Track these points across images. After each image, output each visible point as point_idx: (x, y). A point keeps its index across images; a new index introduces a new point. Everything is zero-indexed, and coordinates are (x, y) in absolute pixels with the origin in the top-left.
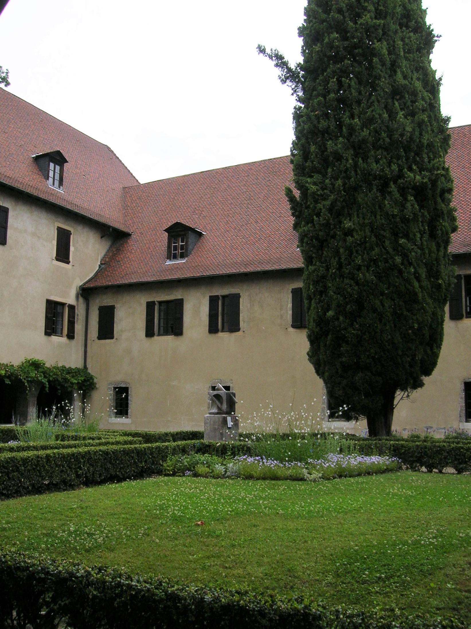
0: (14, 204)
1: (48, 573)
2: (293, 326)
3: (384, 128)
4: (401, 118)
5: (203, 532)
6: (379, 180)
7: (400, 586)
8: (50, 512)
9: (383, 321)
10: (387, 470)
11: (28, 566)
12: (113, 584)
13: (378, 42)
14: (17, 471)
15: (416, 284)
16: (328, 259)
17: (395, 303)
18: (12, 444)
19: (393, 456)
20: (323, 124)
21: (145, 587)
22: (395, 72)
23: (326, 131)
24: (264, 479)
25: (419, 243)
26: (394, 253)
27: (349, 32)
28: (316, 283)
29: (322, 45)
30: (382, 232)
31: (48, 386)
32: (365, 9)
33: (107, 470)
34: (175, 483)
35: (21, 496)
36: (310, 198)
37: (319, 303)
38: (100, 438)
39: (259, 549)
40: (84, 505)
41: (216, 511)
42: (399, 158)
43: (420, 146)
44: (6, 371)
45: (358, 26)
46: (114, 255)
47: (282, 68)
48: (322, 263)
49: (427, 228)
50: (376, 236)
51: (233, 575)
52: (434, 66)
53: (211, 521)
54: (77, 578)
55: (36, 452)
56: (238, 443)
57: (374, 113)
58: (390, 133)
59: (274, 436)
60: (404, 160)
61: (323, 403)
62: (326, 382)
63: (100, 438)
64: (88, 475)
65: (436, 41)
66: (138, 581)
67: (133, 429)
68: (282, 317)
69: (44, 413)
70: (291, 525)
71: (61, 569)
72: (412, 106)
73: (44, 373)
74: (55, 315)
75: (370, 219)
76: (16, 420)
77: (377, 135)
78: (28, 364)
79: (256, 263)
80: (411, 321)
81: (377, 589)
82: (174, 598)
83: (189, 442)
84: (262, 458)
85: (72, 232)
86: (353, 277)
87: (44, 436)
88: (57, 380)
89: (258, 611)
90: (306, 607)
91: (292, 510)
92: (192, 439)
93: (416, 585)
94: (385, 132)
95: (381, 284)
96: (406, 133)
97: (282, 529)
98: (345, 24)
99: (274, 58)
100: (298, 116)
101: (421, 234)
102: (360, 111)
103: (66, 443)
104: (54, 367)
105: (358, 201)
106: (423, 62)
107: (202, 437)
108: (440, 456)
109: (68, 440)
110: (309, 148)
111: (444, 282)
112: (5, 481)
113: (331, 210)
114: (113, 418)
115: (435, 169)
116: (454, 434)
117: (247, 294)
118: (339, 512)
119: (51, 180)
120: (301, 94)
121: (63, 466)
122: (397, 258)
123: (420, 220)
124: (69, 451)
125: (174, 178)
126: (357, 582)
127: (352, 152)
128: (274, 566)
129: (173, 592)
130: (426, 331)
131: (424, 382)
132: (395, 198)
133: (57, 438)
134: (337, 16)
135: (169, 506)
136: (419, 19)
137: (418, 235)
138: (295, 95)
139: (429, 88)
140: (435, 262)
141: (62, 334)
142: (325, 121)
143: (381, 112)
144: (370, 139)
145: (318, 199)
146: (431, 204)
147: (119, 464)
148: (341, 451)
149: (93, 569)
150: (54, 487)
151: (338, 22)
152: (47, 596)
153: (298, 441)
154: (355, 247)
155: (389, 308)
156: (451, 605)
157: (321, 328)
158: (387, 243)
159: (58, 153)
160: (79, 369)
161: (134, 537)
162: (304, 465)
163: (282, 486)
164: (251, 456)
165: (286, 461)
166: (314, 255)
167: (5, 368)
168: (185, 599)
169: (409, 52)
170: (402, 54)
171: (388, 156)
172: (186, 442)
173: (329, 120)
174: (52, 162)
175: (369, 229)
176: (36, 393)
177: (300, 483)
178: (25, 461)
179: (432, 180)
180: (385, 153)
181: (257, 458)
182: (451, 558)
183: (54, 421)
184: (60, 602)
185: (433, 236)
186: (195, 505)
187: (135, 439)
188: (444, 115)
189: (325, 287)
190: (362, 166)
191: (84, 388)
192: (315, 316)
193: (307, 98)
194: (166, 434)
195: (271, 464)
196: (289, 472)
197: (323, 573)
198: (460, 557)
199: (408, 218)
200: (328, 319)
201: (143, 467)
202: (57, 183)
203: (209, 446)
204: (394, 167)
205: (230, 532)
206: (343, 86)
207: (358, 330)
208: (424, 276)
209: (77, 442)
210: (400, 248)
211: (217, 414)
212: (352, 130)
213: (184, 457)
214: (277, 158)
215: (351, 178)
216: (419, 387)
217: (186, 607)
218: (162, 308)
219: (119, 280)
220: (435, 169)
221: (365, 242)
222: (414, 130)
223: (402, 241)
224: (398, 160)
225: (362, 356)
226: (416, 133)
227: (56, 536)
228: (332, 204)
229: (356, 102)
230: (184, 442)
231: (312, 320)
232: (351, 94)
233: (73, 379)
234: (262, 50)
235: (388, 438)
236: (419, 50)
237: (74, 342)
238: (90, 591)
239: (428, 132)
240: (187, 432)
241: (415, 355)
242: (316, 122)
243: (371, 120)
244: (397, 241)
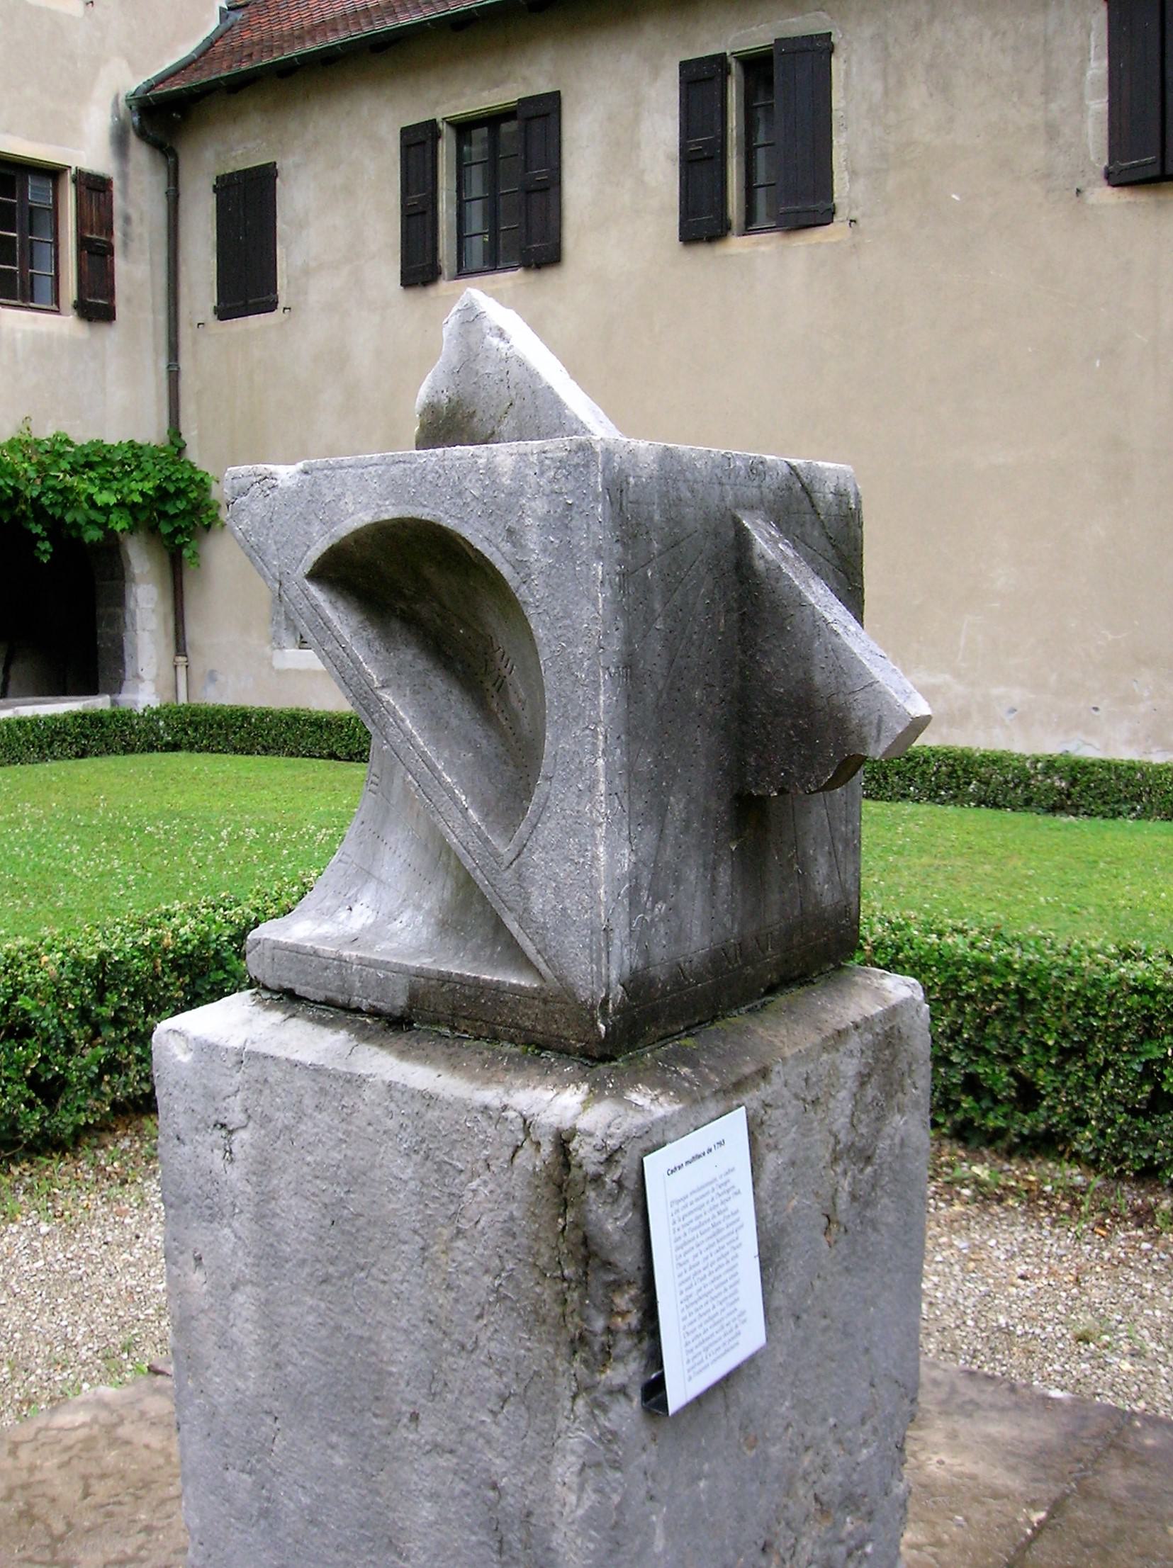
2: (1116, 178)
117: (868, 31)
218: (477, 149)
234: (721, 1143)
237: (111, 336)
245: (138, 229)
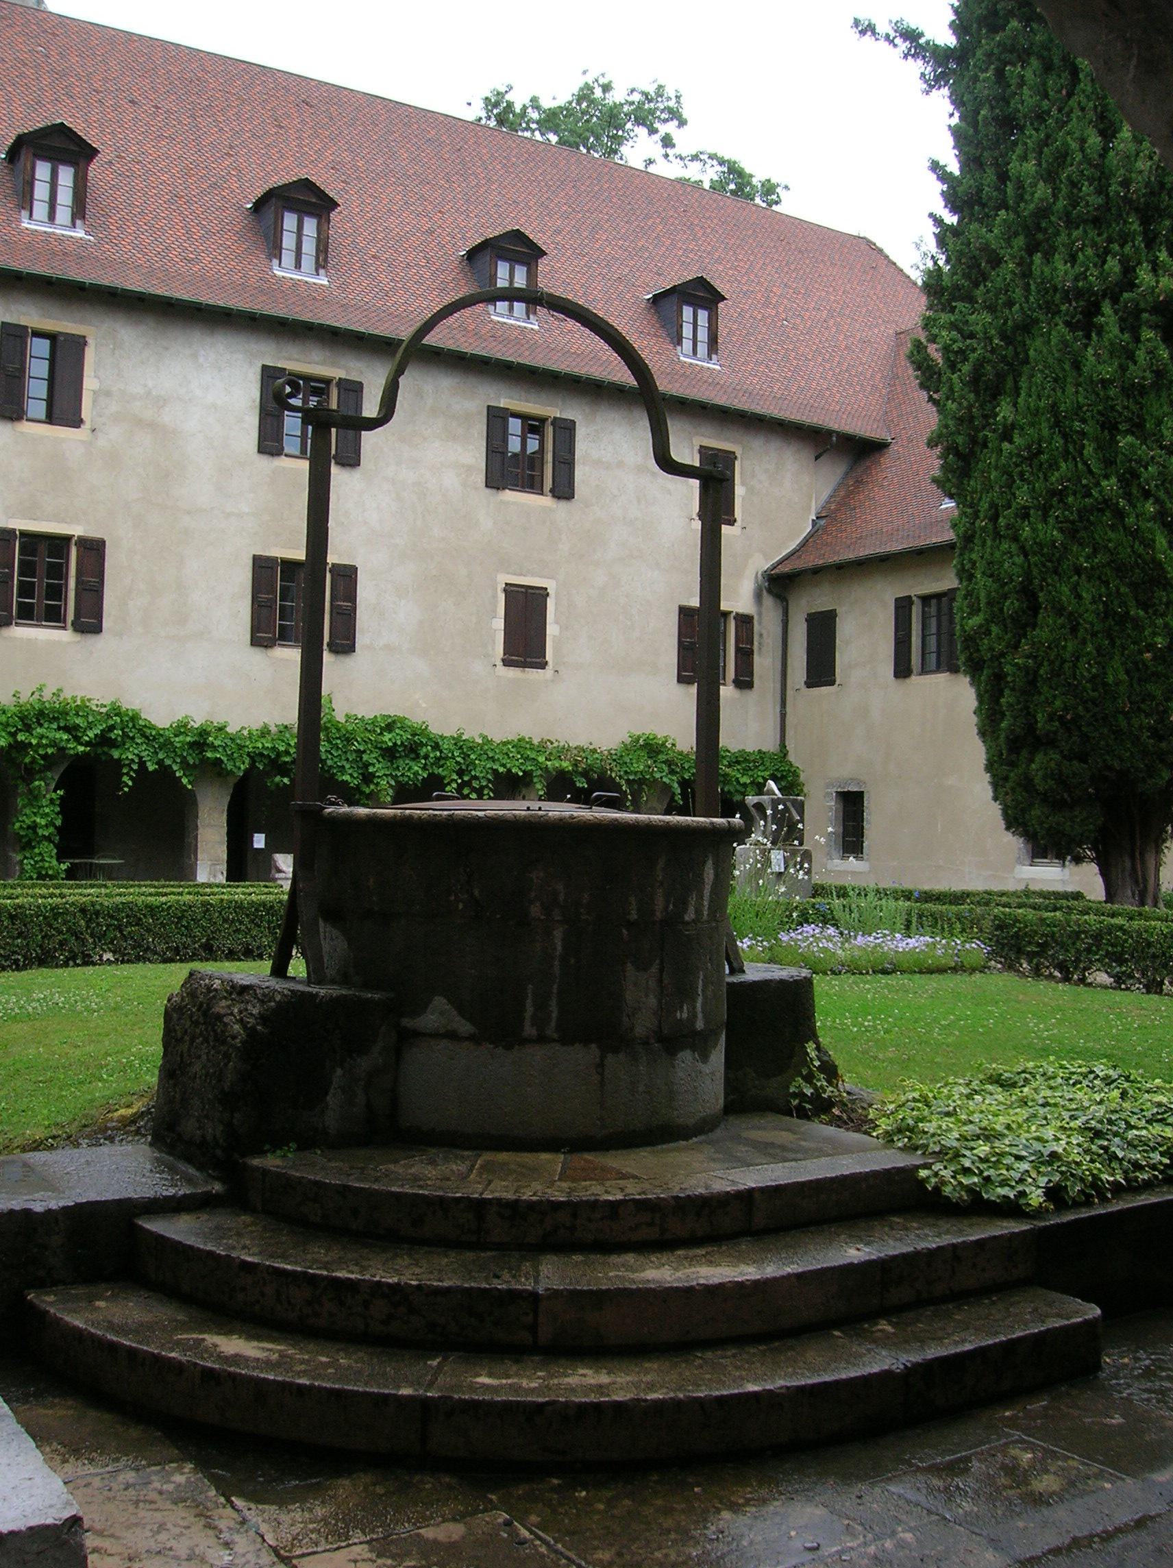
0: (587, 410)
6: (1077, 299)
42: (1124, 239)
50: (1065, 436)
73: (669, 763)
114: (837, 861)
119: (687, 345)
158: (1089, 449)
159: (701, 282)
174: (689, 304)
175: (1048, 420)
180: (1092, 233)
202: (702, 349)
204: (1113, 264)
221: (1040, 452)
223: (1125, 441)
224: (1122, 246)
234: (867, 29)
237: (751, 696)
244: (1114, 441)
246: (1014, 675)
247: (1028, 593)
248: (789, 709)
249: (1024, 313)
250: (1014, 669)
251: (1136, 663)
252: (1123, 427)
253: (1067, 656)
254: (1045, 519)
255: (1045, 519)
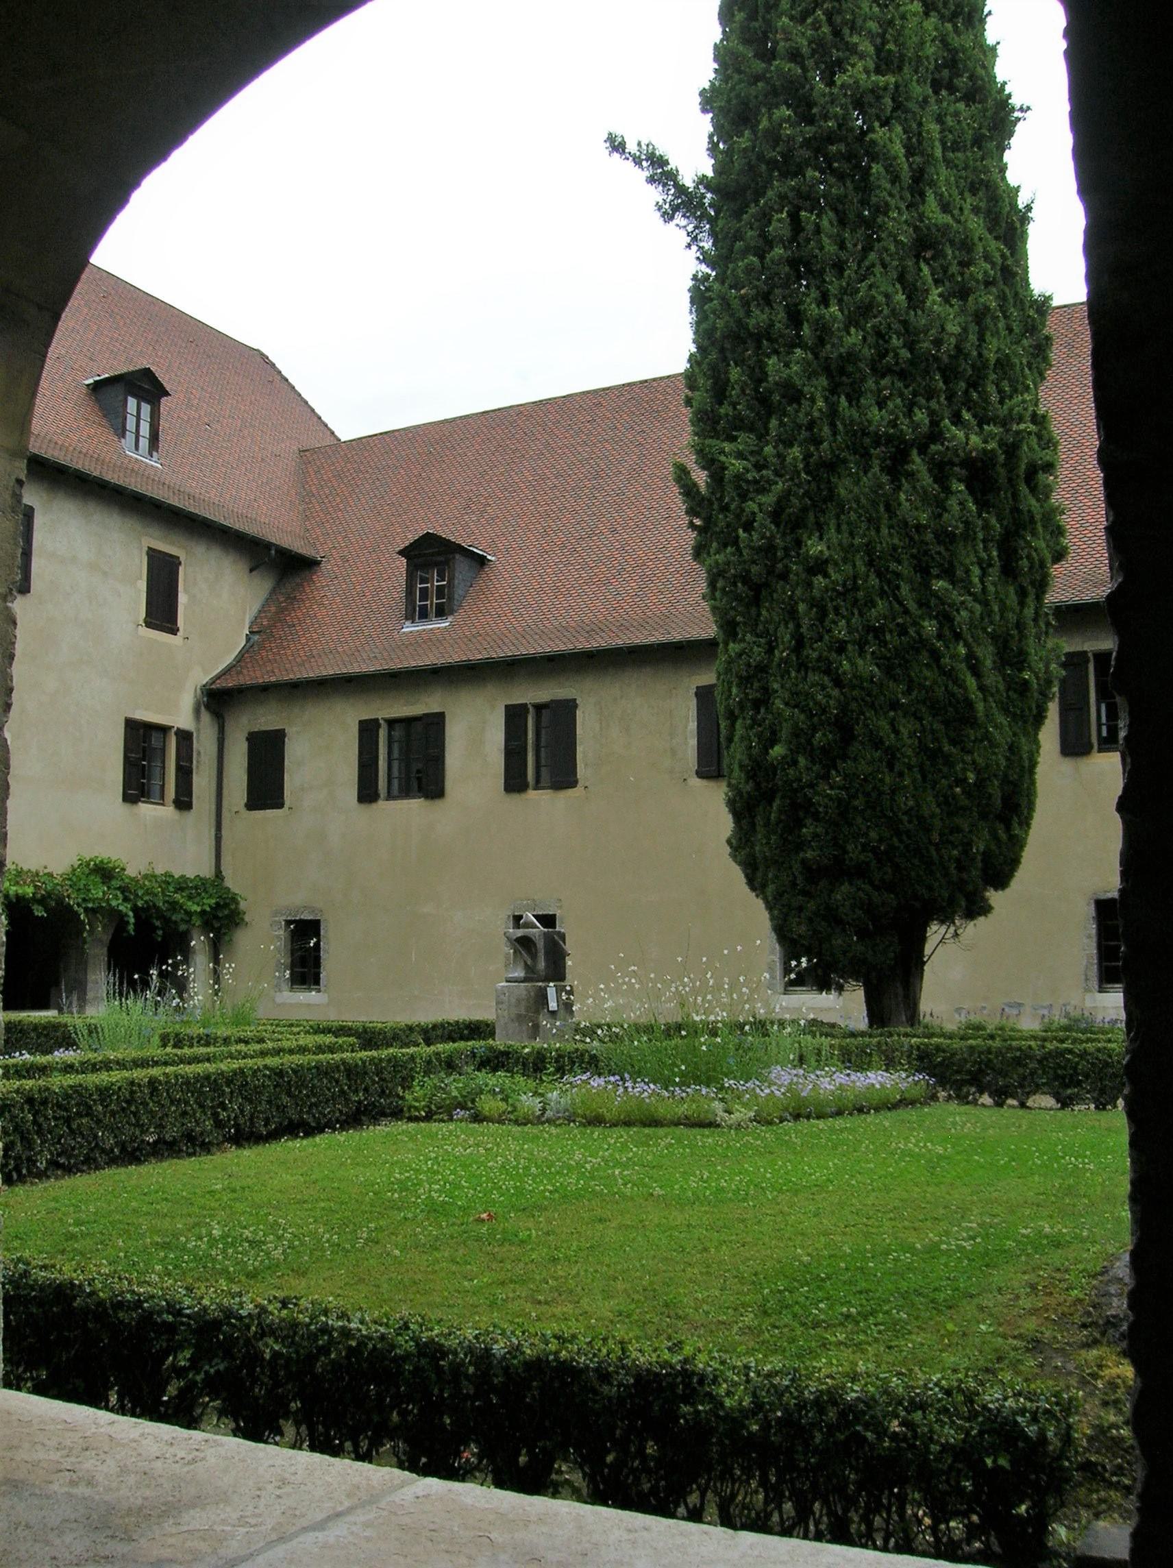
1: (179, 1313)
2: (700, 774)
3: (896, 326)
4: (934, 302)
5: (492, 1234)
6: (886, 445)
7: (887, 1330)
8: (166, 1199)
9: (897, 769)
10: (905, 1102)
11: (139, 1300)
12: (313, 1327)
13: (882, 126)
14: (87, 1115)
15: (971, 682)
16: (771, 628)
17: (922, 725)
18: (61, 1055)
19: (917, 1071)
20: (758, 318)
21: (376, 1331)
22: (922, 195)
23: (763, 336)
24: (628, 1124)
25: (977, 589)
26: (920, 612)
27: (816, 104)
28: (745, 681)
29: (754, 132)
30: (893, 566)
31: (132, 920)
32: (852, 49)
33: (281, 1109)
34: (432, 1136)
35: (98, 1168)
36: (729, 488)
37: (752, 727)
38: (261, 1041)
39: (608, 1266)
40: (237, 1184)
41: (520, 1191)
42: (930, 394)
43: (980, 368)
44: (36, 886)
45: (835, 91)
46: (281, 610)
47: (665, 185)
48: (758, 636)
49: (995, 553)
50: (879, 575)
51: (554, 1316)
52: (1012, 178)
53: (509, 1212)
54: (240, 1318)
55: (126, 1074)
56: (570, 1047)
57: (873, 292)
58: (910, 335)
59: (649, 1029)
60: (942, 399)
61: (772, 953)
62: (770, 908)
63: (261, 1041)
64: (241, 1121)
65: (1018, 119)
66: (362, 1322)
67: (334, 1016)
68: (673, 752)
69: (132, 984)
70: (678, 1218)
71: (208, 1303)
72: (962, 274)
73: (123, 889)
74: (146, 753)
75: (865, 535)
76: (71, 1003)
77: (881, 342)
78: (87, 871)
79: (614, 629)
80: (959, 767)
81: (842, 1337)
82: (432, 1352)
83: (461, 1045)
84: (623, 1079)
85: (182, 559)
86: (828, 670)
87: (135, 1036)
88: (154, 905)
89: (597, 1370)
90: (686, 1361)
91: (682, 1187)
92: (467, 1039)
93: (918, 1327)
94: (899, 335)
95: (891, 684)
96: (946, 337)
97: (658, 1225)
98: (808, 87)
99: (645, 164)
100: (700, 296)
101: (982, 568)
102: (841, 287)
103: (187, 1051)
104: (146, 877)
105: (839, 495)
106: (986, 170)
107: (492, 1034)
108: (1021, 1070)
109: (191, 1046)
110: (727, 372)
111: (1037, 678)
112: (62, 1136)
113: (776, 515)
115: (1012, 419)
116: (1064, 1021)
118: (780, 1191)
119: (130, 437)
120: (707, 245)
121: (187, 1103)
122: (926, 623)
123: (980, 535)
124: (199, 1068)
125: (419, 426)
126: (803, 1324)
127: (823, 381)
128: (636, 1297)
129: (431, 1340)
130: (995, 789)
131: (992, 902)
132: (923, 487)
133: (164, 1040)
134: (787, 66)
135: (420, 1183)
136: (979, 69)
137: (976, 571)
138: (694, 248)
139: (1001, 231)
140: (1014, 632)
141: (162, 798)
142: (762, 311)
143: (890, 289)
144: (867, 352)
145: (748, 490)
146: (1006, 498)
147: (307, 1096)
148: (801, 1060)
149: (270, 1302)
150: (166, 1149)
151: (791, 82)
152: (180, 1356)
153: (702, 1040)
154: (832, 600)
155: (910, 737)
156: (982, 1363)
157: (758, 785)
158: (905, 590)
159: (147, 374)
160: (205, 879)
161: (348, 1246)
162: (716, 1094)
163: (665, 1138)
164: (600, 1075)
165: (677, 1084)
166: (739, 619)
167: (32, 881)
168: (455, 1353)
169: (956, 147)
170: (938, 152)
171: (906, 391)
172: (456, 1045)
173: (772, 308)
174: (134, 396)
175: (862, 558)
176: (106, 938)
177: (706, 1131)
178: (104, 1092)
179: (1006, 445)
180: (900, 384)
181: (612, 1079)
182: (997, 1277)
183: (157, 1004)
184: (207, 1367)
185: (1009, 571)
186: (475, 1181)
187: (340, 1041)
188: (1036, 292)
189: (766, 690)
190: (847, 413)
191: (217, 925)
192: (744, 757)
193: (719, 256)
194: (411, 1028)
195: (643, 1091)
196: (682, 1110)
197: (735, 1310)
198: (1016, 1273)
199: (953, 534)
200: (772, 764)
201: (360, 1102)
202: (144, 443)
203: (506, 1054)
204: (920, 416)
205: (548, 1234)
206: (803, 229)
207: (839, 788)
208: (989, 663)
209: (211, 1049)
210: (933, 602)
211: (525, 980)
212: (823, 331)
213: (452, 1078)
214: (661, 378)
215: (821, 443)
216: (980, 915)
217: (457, 1369)
218: (397, 734)
219: (295, 669)
220: (1012, 419)
221: (856, 588)
222: (965, 330)
223: (939, 585)
224: (928, 400)
225: (850, 847)
226: (971, 336)
227: (184, 1249)
228: (779, 501)
229: (834, 266)
230: (450, 1046)
231: (736, 767)
232: (822, 248)
233: (190, 903)
234: (617, 145)
235: (909, 1030)
236: (978, 141)
237: (191, 816)
238: (267, 1345)
239: (998, 332)
240: (457, 1022)
241: (969, 844)
242: (741, 314)
243: (867, 309)
244: (927, 586)
245: (203, 758)
246: (826, 807)
247: (845, 729)
248: (224, 832)
249: (833, 451)
250: (826, 800)
251: (945, 796)
252: (935, 571)
253: (886, 788)
254: (862, 652)
255: (862, 652)
